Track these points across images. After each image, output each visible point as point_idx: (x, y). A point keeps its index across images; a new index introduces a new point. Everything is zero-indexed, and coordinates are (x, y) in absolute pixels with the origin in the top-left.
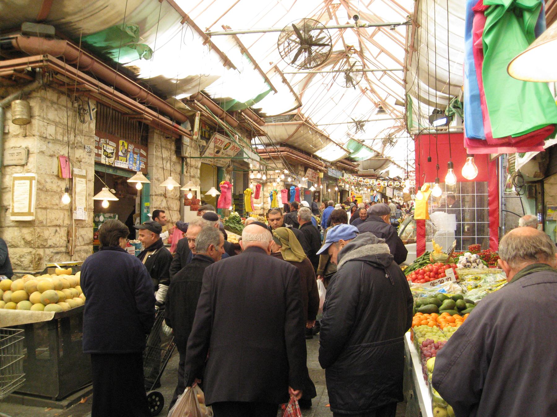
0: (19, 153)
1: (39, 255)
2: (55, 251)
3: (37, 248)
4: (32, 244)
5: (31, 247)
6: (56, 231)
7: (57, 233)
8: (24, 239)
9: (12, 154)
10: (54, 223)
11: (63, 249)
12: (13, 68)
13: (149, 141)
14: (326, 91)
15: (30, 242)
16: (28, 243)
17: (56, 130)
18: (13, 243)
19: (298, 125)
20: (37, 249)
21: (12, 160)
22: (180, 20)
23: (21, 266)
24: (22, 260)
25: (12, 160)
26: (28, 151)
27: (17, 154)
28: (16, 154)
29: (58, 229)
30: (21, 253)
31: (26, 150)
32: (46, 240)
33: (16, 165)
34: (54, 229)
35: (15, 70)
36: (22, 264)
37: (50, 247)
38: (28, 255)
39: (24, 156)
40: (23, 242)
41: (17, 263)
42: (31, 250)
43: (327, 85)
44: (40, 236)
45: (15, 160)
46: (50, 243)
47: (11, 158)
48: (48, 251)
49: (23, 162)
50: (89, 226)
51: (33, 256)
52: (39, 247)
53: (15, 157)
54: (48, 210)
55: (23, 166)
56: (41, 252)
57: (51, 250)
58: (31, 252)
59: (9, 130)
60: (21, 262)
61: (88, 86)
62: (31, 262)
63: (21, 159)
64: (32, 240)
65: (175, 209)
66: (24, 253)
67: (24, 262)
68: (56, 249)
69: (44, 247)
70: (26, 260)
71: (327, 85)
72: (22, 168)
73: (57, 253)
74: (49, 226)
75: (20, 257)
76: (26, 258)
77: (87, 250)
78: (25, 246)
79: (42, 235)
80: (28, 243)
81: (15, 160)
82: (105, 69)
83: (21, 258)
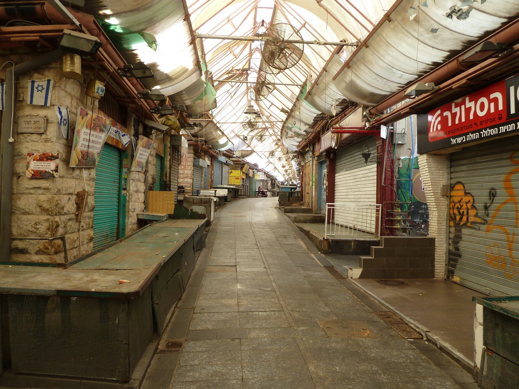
0: (36, 122)
1: (57, 222)
2: (68, 218)
3: (54, 215)
4: (50, 211)
5: (49, 215)
6: (70, 199)
7: (70, 201)
8: (40, 206)
9: (29, 122)
10: (68, 192)
11: (73, 216)
12: (39, 34)
13: (128, 123)
14: (229, 98)
15: (48, 209)
16: (45, 211)
17: (71, 103)
18: (27, 210)
19: (207, 122)
20: (54, 216)
21: (28, 128)
22: (183, 17)
23: (37, 233)
24: (38, 227)
25: (28, 128)
26: (47, 120)
27: (34, 122)
28: (33, 122)
29: (71, 196)
30: (37, 221)
31: (45, 119)
32: (63, 208)
33: (32, 134)
34: (68, 196)
35: (40, 36)
36: (38, 232)
37: (65, 214)
38: (44, 222)
39: (43, 125)
40: (38, 209)
41: (31, 230)
42: (48, 217)
43: (231, 93)
44: (58, 204)
45: (31, 128)
46: (65, 210)
47: (27, 126)
48: (64, 218)
49: (42, 131)
50: (92, 194)
51: (51, 223)
52: (56, 215)
53: (32, 125)
54: (64, 179)
55: (41, 134)
56: (57, 218)
57: (65, 216)
58: (48, 219)
59: (23, 98)
60: (36, 229)
61: (106, 64)
62: (49, 229)
63: (40, 128)
64: (50, 208)
65: (142, 181)
66: (40, 220)
67: (40, 229)
68: (68, 215)
69: (60, 214)
70: (42, 227)
71: (231, 93)
72: (39, 136)
73: (70, 220)
74: (64, 194)
75: (36, 224)
76: (42, 225)
77: (90, 216)
78: (41, 214)
79: (59, 202)
80: (45, 211)
81: (31, 128)
82: (114, 53)
83: (37, 225)
